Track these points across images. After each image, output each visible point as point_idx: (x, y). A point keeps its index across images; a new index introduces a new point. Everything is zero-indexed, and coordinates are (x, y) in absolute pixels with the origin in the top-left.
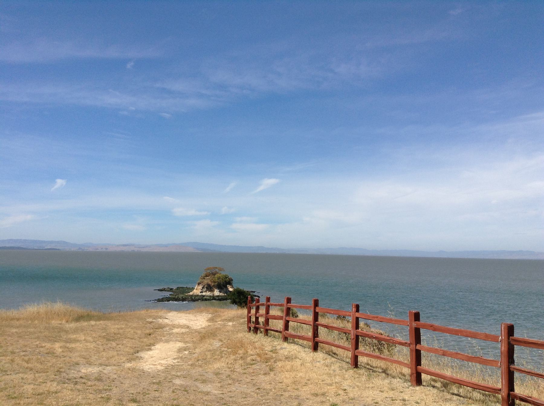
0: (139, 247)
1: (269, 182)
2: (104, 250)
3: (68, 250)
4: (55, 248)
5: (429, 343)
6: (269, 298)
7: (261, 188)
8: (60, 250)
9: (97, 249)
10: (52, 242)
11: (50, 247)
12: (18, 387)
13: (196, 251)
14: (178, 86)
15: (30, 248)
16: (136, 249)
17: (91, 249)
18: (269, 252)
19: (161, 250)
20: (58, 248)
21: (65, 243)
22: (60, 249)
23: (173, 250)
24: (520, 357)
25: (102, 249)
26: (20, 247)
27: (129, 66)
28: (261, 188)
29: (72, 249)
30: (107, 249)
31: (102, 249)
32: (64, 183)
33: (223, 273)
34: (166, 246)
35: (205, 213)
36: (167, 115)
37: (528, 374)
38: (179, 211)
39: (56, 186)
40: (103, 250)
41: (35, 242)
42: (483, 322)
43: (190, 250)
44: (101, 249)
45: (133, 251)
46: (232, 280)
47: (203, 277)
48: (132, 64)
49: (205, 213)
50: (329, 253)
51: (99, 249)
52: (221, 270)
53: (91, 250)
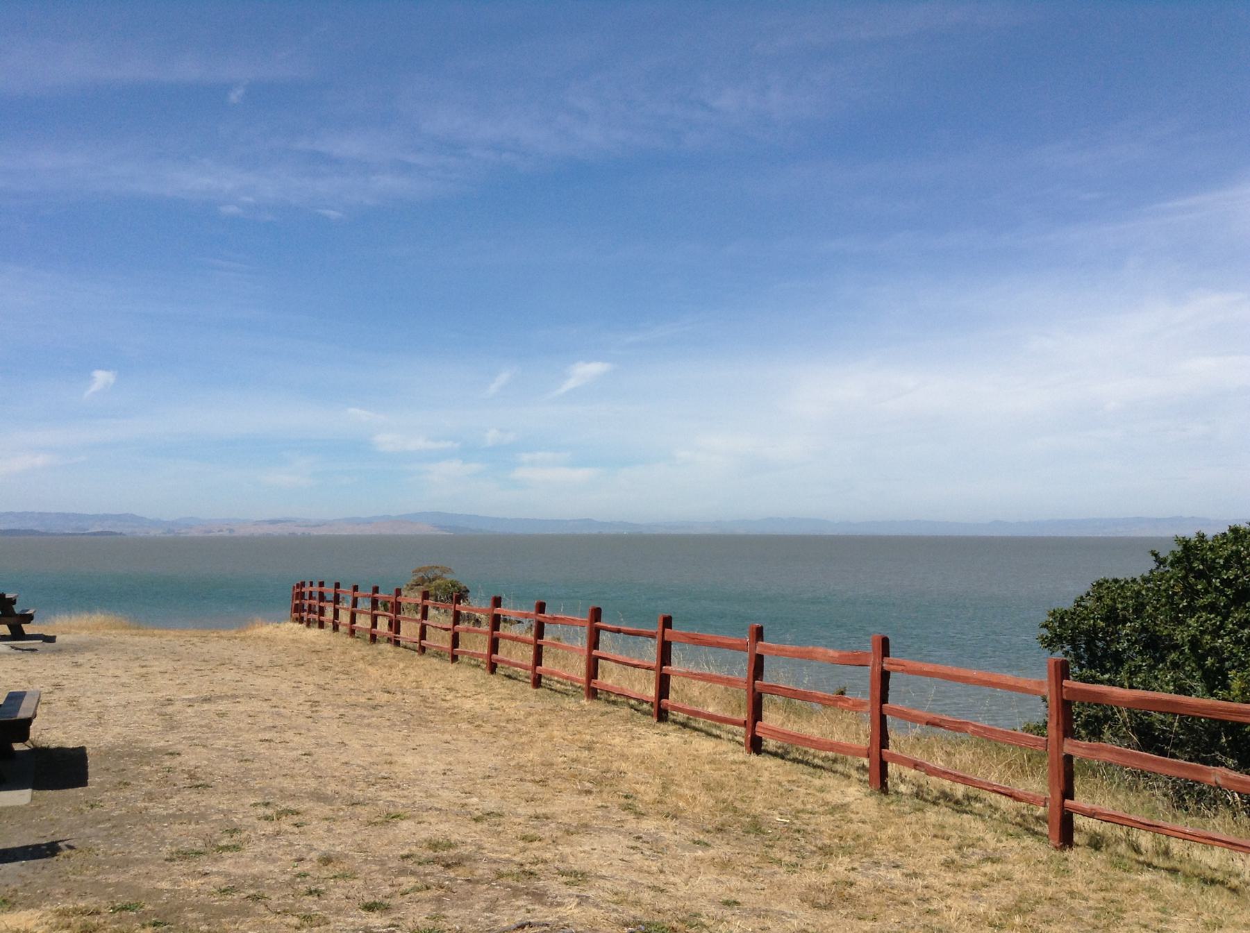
0: (306, 526)
1: (587, 371)
2: (226, 533)
3: (141, 535)
4: (111, 530)
5: (1009, 698)
6: (762, 628)
7: (571, 384)
8: (124, 535)
9: (210, 532)
10: (105, 518)
11: (100, 530)
12: (100, 846)
13: (438, 533)
14: (349, 146)
15: (54, 532)
16: (299, 531)
17: (194, 533)
18: (606, 531)
19: (358, 531)
20: (117, 530)
21: (133, 517)
22: (124, 532)
23: (387, 531)
24: (1191, 674)
25: (221, 531)
26: (32, 530)
27: (234, 97)
28: (571, 384)
29: (152, 533)
30: (231, 531)
31: (221, 531)
32: (112, 380)
33: (450, 577)
34: (368, 522)
35: (449, 444)
36: (333, 214)
37: (1147, 831)
38: (387, 441)
39: (95, 388)
40: (221, 533)
41: (65, 516)
42: (497, 848)
43: (425, 529)
44: (219, 531)
45: (293, 534)
46: (468, 591)
47: (410, 586)
48: (240, 92)
49: (449, 444)
50: (741, 531)
51: (214, 532)
52: (449, 570)
53: (196, 534)
